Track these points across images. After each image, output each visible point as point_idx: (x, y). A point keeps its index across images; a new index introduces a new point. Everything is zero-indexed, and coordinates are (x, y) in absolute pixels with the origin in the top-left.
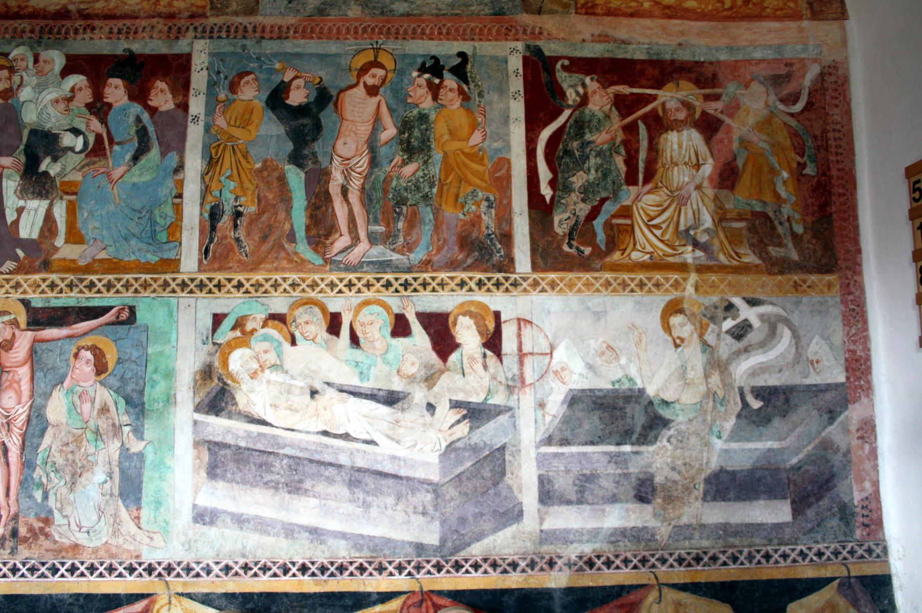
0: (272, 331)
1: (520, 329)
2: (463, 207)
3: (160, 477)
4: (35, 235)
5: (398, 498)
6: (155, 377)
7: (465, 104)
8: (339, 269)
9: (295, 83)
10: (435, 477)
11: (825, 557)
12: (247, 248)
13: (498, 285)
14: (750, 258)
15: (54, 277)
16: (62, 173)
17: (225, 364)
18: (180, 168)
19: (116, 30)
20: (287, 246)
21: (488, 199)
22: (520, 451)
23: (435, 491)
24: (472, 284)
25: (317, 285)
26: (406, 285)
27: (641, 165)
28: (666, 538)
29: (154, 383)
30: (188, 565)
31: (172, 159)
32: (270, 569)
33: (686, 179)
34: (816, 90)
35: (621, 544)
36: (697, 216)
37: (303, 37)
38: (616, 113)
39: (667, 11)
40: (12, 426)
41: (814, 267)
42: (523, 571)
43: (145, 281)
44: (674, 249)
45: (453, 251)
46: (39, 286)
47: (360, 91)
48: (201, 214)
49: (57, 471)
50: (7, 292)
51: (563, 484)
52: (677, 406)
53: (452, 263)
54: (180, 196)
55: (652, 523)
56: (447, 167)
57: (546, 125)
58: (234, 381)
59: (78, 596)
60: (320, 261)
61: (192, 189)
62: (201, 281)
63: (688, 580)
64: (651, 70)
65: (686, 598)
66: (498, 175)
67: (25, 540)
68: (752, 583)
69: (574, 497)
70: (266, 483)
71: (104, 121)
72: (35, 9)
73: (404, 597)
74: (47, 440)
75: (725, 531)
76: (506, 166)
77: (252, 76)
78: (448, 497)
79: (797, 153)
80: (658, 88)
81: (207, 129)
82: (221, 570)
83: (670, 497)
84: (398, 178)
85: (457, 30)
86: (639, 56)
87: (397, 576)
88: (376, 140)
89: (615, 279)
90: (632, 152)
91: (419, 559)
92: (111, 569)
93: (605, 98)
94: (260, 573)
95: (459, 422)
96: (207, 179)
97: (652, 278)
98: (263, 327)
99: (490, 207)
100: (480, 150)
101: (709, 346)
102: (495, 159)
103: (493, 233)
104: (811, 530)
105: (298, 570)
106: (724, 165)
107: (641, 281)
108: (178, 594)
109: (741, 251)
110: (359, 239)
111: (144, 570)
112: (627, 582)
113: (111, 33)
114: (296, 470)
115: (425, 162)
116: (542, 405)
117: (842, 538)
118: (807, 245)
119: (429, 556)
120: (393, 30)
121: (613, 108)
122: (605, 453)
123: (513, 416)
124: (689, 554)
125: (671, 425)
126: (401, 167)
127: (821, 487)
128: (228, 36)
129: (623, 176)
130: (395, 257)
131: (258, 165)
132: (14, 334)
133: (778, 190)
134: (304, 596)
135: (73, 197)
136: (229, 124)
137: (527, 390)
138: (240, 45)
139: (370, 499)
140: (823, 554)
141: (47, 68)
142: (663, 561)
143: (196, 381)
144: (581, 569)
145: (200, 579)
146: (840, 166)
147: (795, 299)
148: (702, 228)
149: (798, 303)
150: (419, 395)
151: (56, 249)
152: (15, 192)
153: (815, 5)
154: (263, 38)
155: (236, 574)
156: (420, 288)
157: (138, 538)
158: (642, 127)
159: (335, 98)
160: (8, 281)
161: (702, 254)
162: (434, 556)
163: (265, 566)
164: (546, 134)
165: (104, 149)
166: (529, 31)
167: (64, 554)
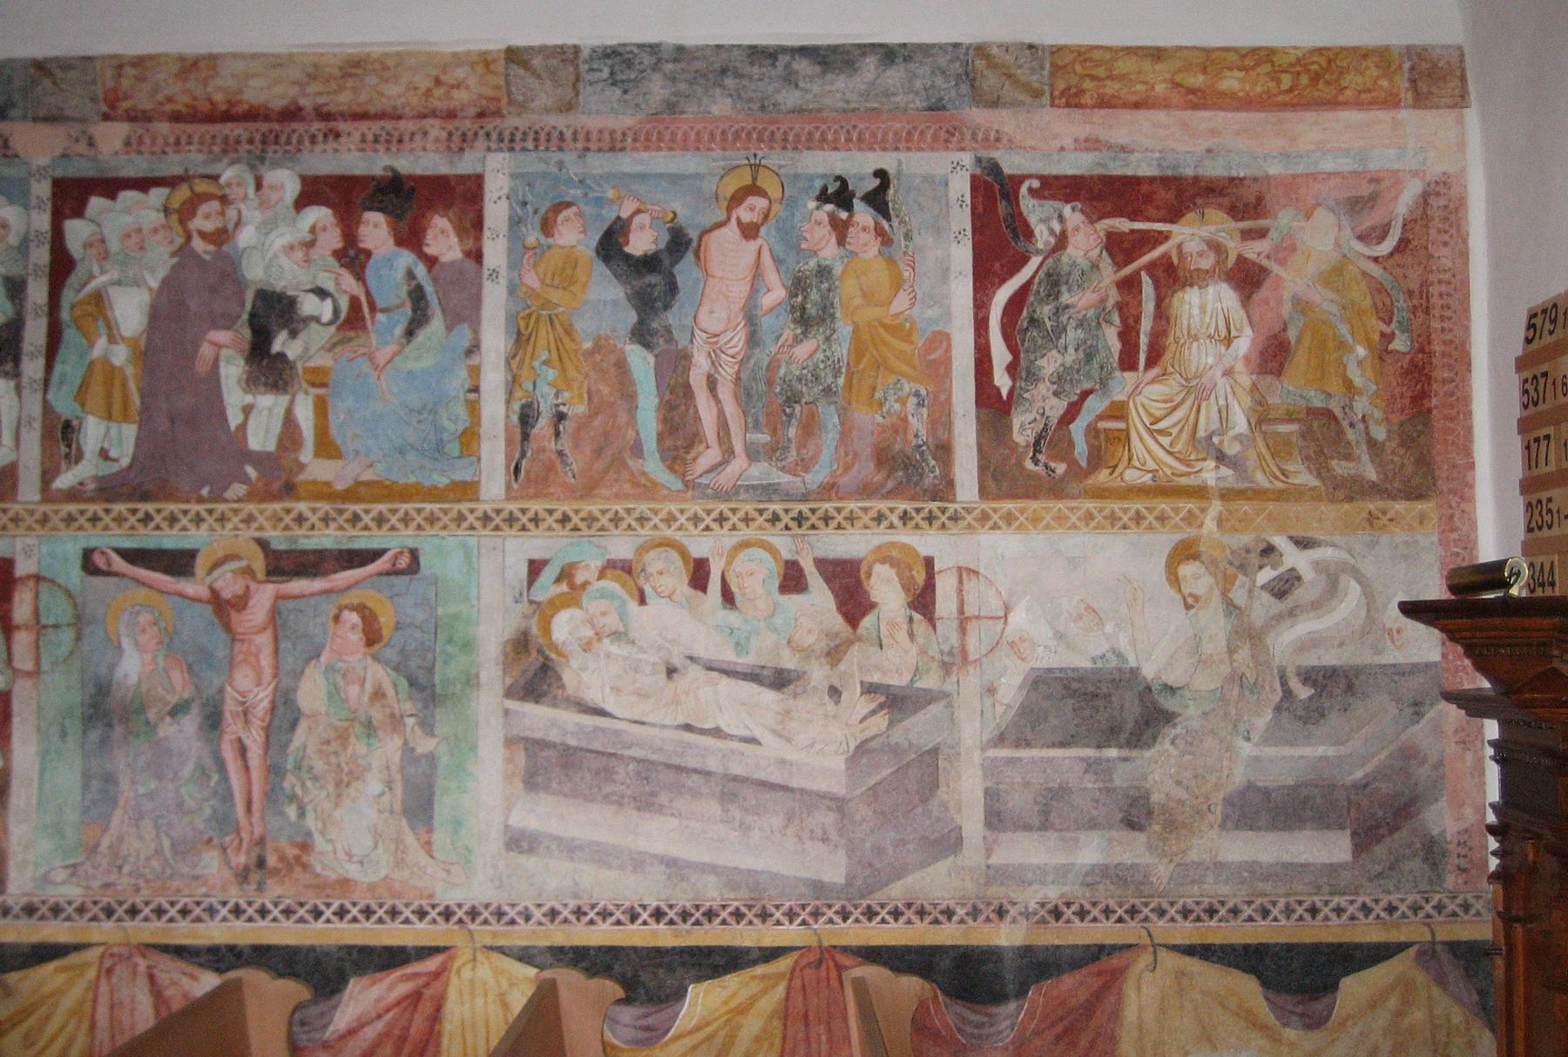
0: (610, 585)
1: (961, 582)
2: (881, 405)
3: (459, 787)
4: (271, 446)
5: (790, 818)
6: (449, 648)
7: (885, 250)
8: (705, 496)
9: (637, 220)
10: (838, 787)
11: (1399, 913)
12: (574, 466)
13: (930, 519)
14: (1304, 477)
15: (302, 507)
16: (305, 355)
17: (547, 631)
18: (474, 348)
19: (370, 137)
20: (630, 463)
21: (917, 394)
22: (959, 754)
23: (840, 810)
24: (895, 519)
25: (675, 520)
26: (800, 519)
27: (1144, 341)
28: (1165, 881)
29: (449, 658)
30: (499, 907)
31: (463, 335)
32: (611, 914)
33: (1210, 360)
34: (1415, 221)
35: (1101, 886)
36: (1224, 415)
37: (647, 148)
38: (1109, 260)
39: (1191, 97)
40: (250, 716)
41: (1400, 491)
42: (962, 921)
43: (432, 513)
44: (1188, 466)
45: (866, 469)
46: (281, 520)
47: (731, 231)
48: (507, 416)
49: (315, 779)
50: (236, 528)
51: (1019, 801)
52: (1187, 693)
53: (866, 487)
54: (476, 389)
55: (1146, 859)
56: (858, 350)
57: (1003, 281)
58: (560, 654)
59: (349, 949)
60: (678, 485)
61: (493, 379)
62: (511, 513)
63: (1196, 940)
64: (1163, 193)
65: (1194, 965)
66: (932, 357)
67: (275, 872)
68: (1290, 948)
69: (1036, 822)
70: (606, 797)
71: (360, 277)
72: (251, 106)
73: (795, 955)
74: (300, 736)
75: (1252, 872)
76: (945, 344)
77: (574, 209)
78: (858, 817)
79: (1381, 319)
80: (1172, 222)
81: (512, 290)
82: (545, 915)
83: (1172, 822)
84: (788, 363)
85: (874, 135)
86: (1146, 170)
87: (787, 926)
88: (756, 307)
89: (1022, 511)
90: (1131, 321)
91: (818, 903)
92: (394, 913)
93: (1091, 238)
94: (598, 919)
95: (873, 713)
96: (514, 366)
97: (1154, 508)
98: (600, 578)
99: (920, 404)
100: (906, 320)
101: (1235, 607)
102: (928, 333)
103: (924, 444)
104: (1379, 875)
105: (651, 916)
106: (1268, 339)
107: (1138, 512)
108: (485, 947)
109: (1289, 467)
110: (733, 452)
111: (439, 914)
112: (1108, 941)
113: (364, 141)
114: (646, 778)
115: (828, 339)
116: (991, 690)
117: (1424, 886)
118: (1390, 457)
119: (832, 898)
120: (779, 135)
121: (1104, 252)
122: (1082, 759)
123: (950, 706)
124: (1198, 903)
125: (1177, 721)
126: (792, 346)
127: (1397, 814)
128: (536, 147)
129: (1116, 357)
130: (785, 478)
131: (588, 345)
132: (248, 588)
133: (1349, 373)
134: (659, 952)
135: (321, 391)
136: (542, 282)
137: (971, 669)
138: (554, 160)
139: (749, 818)
140: (1396, 908)
141: (274, 196)
142: (1161, 913)
143: (506, 655)
144: (1043, 921)
145: (516, 927)
146: (1448, 337)
147: (1368, 538)
148: (1232, 433)
149: (1373, 544)
150: (819, 674)
151: (302, 467)
152: (239, 382)
153: (1420, 83)
154: (587, 149)
155: (566, 920)
156: (820, 524)
157: (430, 871)
158: (1145, 278)
159: (695, 244)
160: (236, 512)
161: (1232, 472)
162: (839, 898)
163: (605, 910)
164: (1003, 295)
165: (363, 319)
166: (980, 136)
167: (329, 891)
